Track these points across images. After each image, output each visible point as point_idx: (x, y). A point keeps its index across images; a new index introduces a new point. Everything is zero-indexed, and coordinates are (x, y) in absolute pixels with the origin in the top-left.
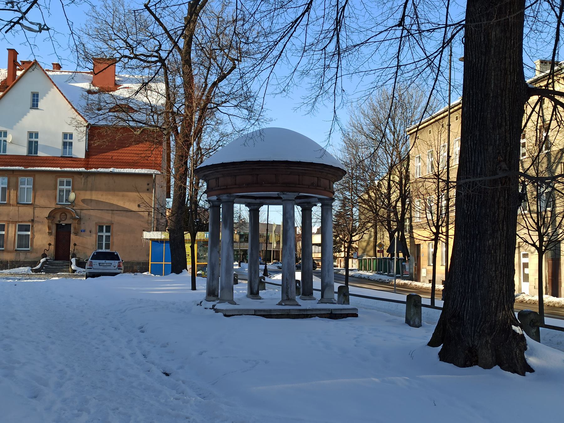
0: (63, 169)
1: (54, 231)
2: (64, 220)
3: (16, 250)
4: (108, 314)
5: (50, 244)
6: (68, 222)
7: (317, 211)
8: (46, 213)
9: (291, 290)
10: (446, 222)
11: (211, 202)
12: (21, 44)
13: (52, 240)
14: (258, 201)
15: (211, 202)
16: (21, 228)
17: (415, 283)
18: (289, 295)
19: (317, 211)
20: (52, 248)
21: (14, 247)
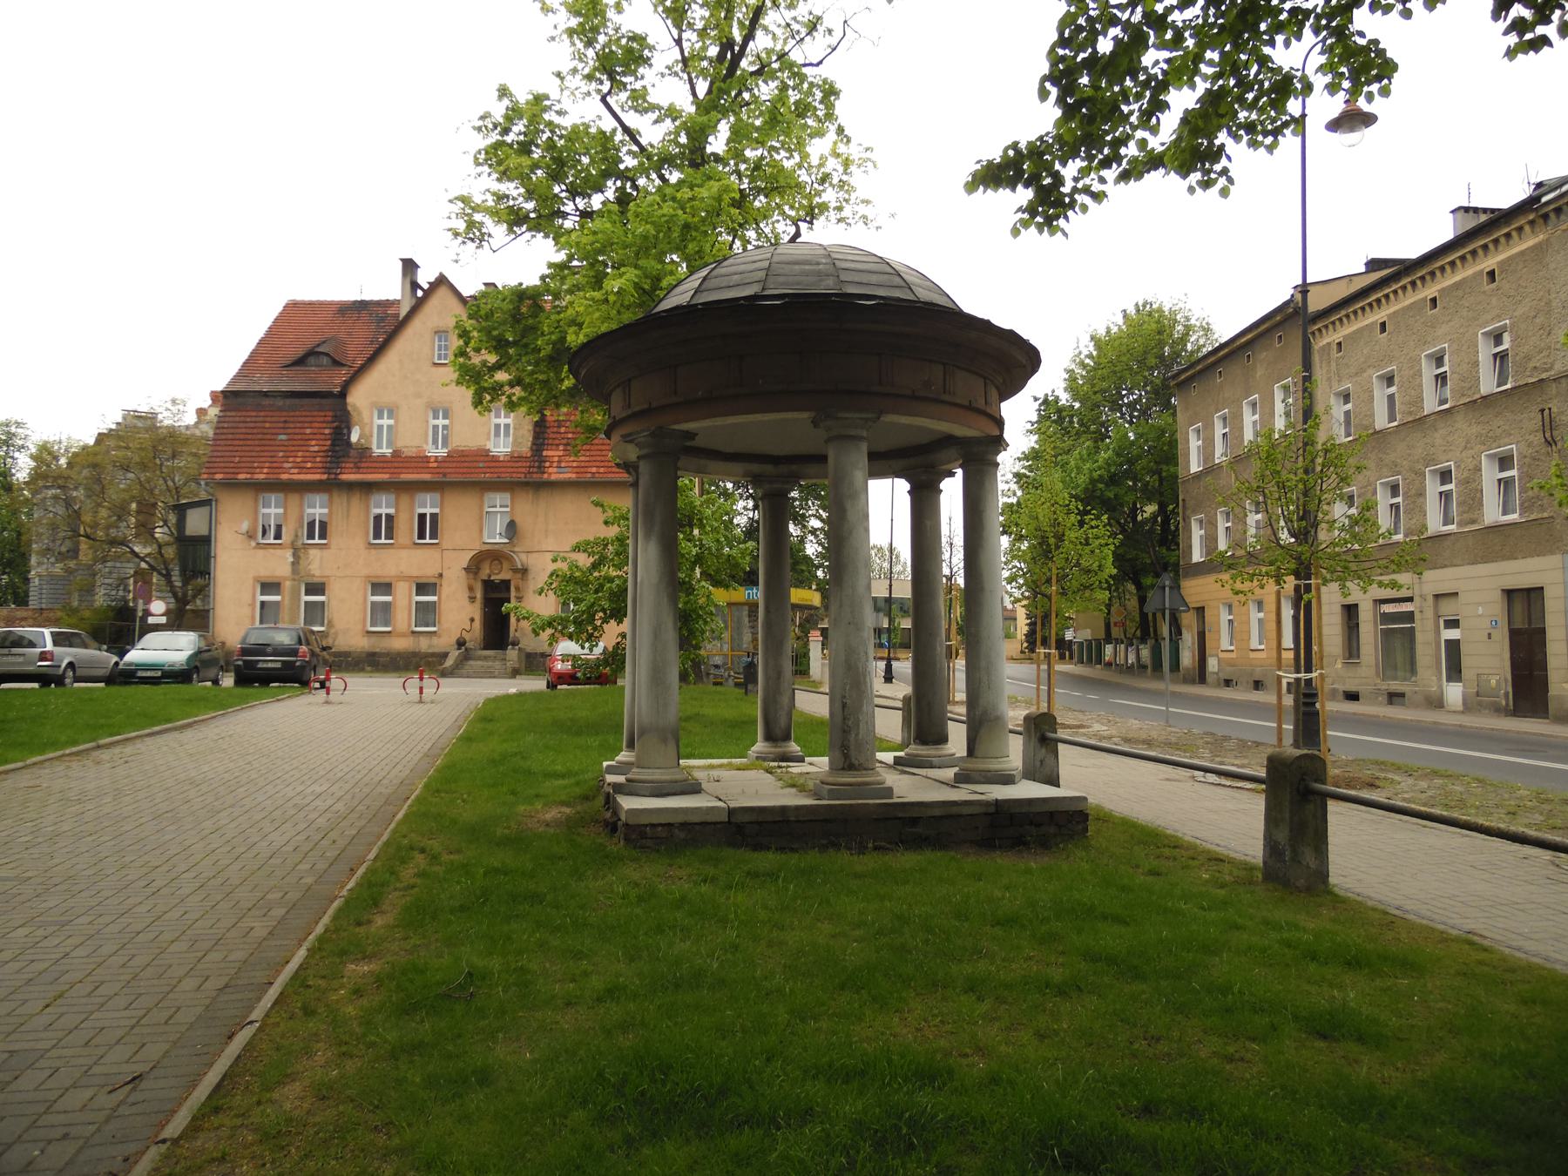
0: (1310, 752)
1: (479, 594)
2: (497, 574)
3: (413, 632)
4: (1425, 560)
5: (472, 620)
6: (505, 575)
7: (952, 490)
8: (465, 559)
9: (857, 735)
10: (532, 804)
11: (631, 470)
12: (451, 201)
13: (476, 611)
14: (784, 469)
15: (631, 470)
16: (422, 588)
17: (1323, 786)
18: (853, 753)
19: (952, 490)
20: (477, 625)
21: (410, 625)
